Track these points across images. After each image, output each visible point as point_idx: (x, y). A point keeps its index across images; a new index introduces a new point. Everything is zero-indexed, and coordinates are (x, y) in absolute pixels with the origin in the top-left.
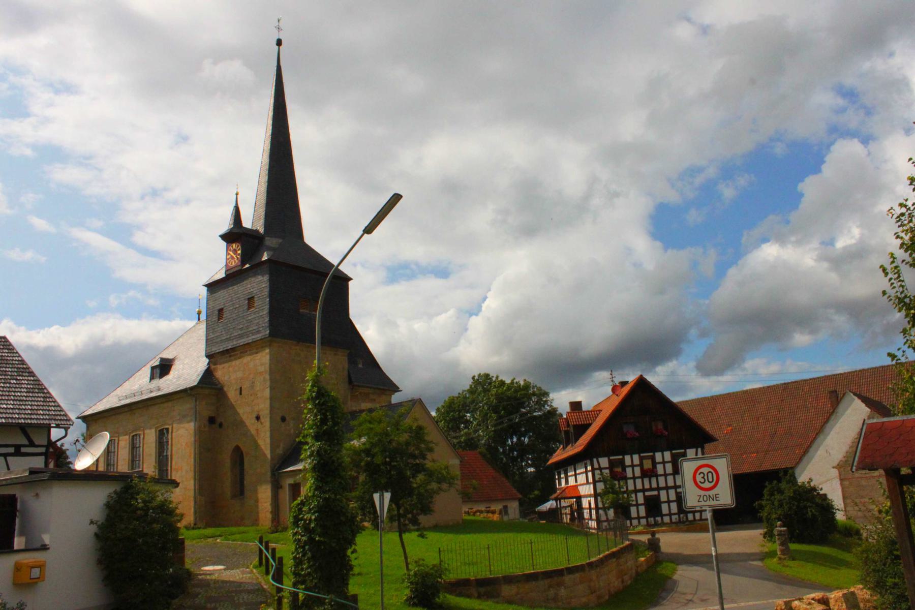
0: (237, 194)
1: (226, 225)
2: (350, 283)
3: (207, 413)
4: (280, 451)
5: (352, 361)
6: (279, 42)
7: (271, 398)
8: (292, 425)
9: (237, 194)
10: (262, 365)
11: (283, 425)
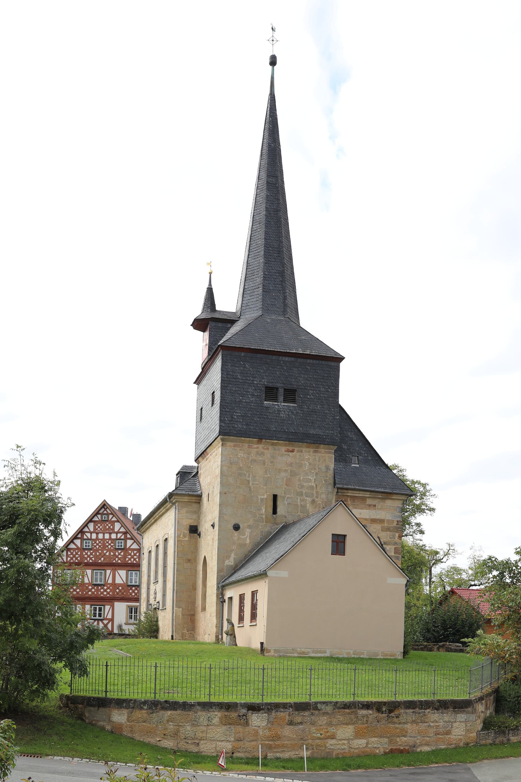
0: (210, 273)
1: (197, 310)
5: (341, 458)
6: (273, 62)
9: (210, 273)
11: (236, 533)
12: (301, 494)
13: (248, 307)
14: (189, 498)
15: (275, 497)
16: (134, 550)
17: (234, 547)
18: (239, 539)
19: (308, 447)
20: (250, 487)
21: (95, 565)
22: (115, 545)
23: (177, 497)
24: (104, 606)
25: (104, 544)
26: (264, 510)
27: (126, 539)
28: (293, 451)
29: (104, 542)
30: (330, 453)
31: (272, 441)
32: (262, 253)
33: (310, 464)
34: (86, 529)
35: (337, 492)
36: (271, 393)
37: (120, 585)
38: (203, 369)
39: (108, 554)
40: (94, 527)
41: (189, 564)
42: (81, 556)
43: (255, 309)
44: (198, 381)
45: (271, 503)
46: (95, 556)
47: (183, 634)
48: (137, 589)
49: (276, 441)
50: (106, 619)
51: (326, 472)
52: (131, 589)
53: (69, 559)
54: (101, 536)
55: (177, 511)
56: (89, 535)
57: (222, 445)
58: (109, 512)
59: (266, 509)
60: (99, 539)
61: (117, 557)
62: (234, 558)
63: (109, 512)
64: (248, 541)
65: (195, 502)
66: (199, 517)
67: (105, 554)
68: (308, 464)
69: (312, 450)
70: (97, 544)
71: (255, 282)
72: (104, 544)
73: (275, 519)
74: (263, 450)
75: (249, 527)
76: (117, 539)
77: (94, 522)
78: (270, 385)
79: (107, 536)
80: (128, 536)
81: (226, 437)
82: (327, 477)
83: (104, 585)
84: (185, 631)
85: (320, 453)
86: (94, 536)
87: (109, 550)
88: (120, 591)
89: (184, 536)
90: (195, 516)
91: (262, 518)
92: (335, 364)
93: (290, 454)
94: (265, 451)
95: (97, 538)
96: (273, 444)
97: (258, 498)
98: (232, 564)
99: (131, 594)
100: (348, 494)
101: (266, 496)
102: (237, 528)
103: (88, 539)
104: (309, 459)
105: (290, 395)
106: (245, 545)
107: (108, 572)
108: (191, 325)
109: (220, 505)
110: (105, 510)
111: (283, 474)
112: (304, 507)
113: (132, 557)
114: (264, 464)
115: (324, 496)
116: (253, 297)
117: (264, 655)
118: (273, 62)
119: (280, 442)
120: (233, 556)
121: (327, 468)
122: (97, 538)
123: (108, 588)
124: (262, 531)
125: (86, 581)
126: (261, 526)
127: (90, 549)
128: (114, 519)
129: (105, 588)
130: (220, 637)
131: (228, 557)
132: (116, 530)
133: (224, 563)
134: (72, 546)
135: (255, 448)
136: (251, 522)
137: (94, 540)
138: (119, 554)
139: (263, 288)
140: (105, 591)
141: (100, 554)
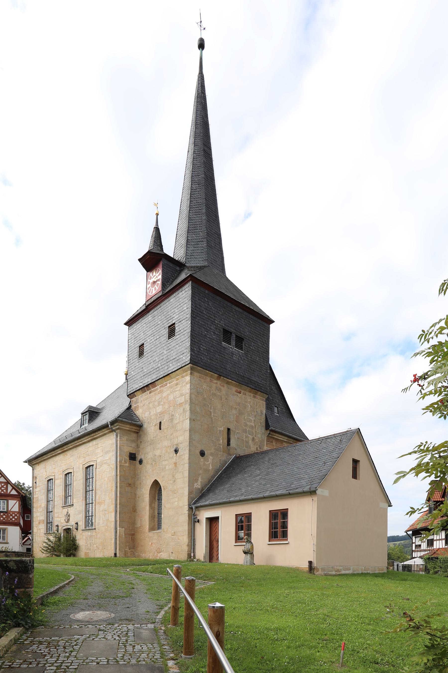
0: (157, 214)
1: (145, 247)
2: (271, 326)
3: (129, 449)
4: (198, 485)
5: (269, 407)
6: (201, 46)
7: (191, 430)
8: (210, 461)
9: (157, 214)
11: (202, 459)
13: (193, 257)
14: (131, 427)
15: (229, 429)
17: (201, 472)
18: (204, 464)
19: (250, 392)
20: (212, 418)
23: (120, 424)
26: (221, 441)
30: (263, 400)
31: (228, 380)
32: (204, 211)
33: (251, 407)
35: (269, 434)
36: (227, 335)
38: (147, 307)
41: (129, 488)
43: (200, 259)
44: (130, 323)
47: (125, 551)
48: (5, 515)
49: (230, 381)
51: (261, 415)
55: (119, 437)
57: (191, 374)
59: (222, 441)
64: (211, 467)
65: (134, 432)
66: (138, 447)
68: (250, 406)
69: (252, 395)
71: (198, 235)
73: (229, 450)
74: (220, 386)
75: (212, 454)
78: (227, 328)
81: (195, 366)
82: (261, 420)
84: (127, 549)
85: (257, 399)
89: (125, 462)
90: (134, 445)
91: (220, 447)
92: (266, 324)
93: (239, 394)
94: (222, 388)
96: (228, 383)
97: (217, 429)
98: (200, 487)
99: (11, 519)
100: (275, 437)
101: (223, 428)
102: (202, 454)
104: (250, 402)
105: (240, 341)
106: (209, 470)
108: (140, 260)
109: (190, 430)
112: (248, 442)
114: (221, 400)
115: (259, 436)
117: (314, 574)
118: (201, 46)
119: (233, 382)
120: (200, 479)
124: (220, 460)
126: (220, 455)
130: (192, 554)
131: (197, 480)
133: (194, 485)
135: (214, 383)
136: (213, 451)
139: (207, 243)
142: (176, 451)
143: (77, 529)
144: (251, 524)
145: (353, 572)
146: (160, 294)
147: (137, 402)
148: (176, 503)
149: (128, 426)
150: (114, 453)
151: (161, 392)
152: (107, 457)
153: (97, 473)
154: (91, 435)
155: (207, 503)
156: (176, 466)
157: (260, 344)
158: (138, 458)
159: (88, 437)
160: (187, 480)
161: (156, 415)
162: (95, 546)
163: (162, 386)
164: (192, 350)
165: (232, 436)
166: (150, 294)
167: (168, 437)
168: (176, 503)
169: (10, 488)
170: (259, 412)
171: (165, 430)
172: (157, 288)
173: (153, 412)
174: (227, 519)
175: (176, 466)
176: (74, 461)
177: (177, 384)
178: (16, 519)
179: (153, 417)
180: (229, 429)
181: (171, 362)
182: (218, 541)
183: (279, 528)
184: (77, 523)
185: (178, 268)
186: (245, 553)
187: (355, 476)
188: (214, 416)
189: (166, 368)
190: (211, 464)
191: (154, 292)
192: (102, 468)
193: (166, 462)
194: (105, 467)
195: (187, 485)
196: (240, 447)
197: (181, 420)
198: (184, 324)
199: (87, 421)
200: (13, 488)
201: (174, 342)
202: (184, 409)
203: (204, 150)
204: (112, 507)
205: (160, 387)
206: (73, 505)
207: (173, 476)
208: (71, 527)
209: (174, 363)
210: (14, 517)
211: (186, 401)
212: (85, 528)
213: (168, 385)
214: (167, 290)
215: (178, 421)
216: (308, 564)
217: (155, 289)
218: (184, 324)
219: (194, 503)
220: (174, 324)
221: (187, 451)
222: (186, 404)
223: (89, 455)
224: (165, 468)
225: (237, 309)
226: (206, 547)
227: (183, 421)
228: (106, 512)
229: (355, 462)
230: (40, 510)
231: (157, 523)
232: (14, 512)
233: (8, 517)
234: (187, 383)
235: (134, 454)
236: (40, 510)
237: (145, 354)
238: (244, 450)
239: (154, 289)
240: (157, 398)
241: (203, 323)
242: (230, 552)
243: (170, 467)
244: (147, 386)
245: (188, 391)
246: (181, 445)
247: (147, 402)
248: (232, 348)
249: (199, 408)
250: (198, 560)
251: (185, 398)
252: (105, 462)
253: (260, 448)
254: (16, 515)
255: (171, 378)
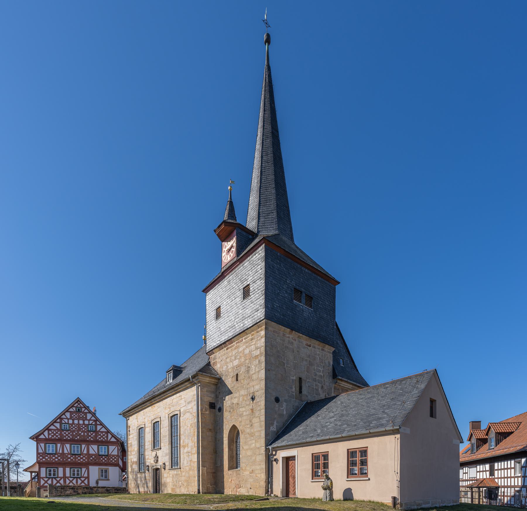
4: (273, 428)
10: (257, 348)
11: (277, 405)
12: (315, 380)
14: (211, 380)
15: (300, 379)
16: (102, 432)
19: (319, 345)
20: (285, 368)
21: (72, 441)
22: (88, 428)
24: (81, 468)
25: (79, 427)
27: (96, 425)
28: (310, 346)
29: (79, 426)
30: (330, 353)
33: (320, 358)
34: (64, 417)
36: (297, 292)
37: (93, 455)
39: (82, 434)
40: (71, 415)
42: (61, 434)
45: (298, 384)
46: (72, 435)
50: (83, 477)
52: (102, 457)
53: (50, 436)
54: (76, 422)
56: (66, 421)
58: (82, 406)
59: (294, 389)
60: (75, 424)
61: (90, 436)
62: (276, 426)
63: (82, 406)
64: (285, 413)
67: (80, 434)
69: (321, 348)
70: (74, 427)
72: (79, 427)
75: (286, 401)
76: (89, 424)
77: (70, 412)
79: (81, 422)
80: (98, 423)
83: (80, 455)
86: (71, 422)
87: (84, 432)
88: (93, 458)
89: (206, 410)
93: (309, 348)
95: (73, 423)
102: (277, 400)
103: (66, 423)
104: (319, 354)
105: (310, 299)
107: (83, 446)
110: (79, 404)
111: (304, 362)
112: (317, 390)
113: (102, 437)
114: (293, 352)
115: (327, 384)
116: (267, 219)
120: (275, 422)
121: (329, 363)
122: (73, 423)
123: (84, 457)
125: (66, 451)
127: (68, 430)
128: (86, 411)
129: (82, 456)
131: (272, 424)
132: (88, 418)
134: (52, 427)
137: (70, 424)
138: (92, 434)
140: (82, 458)
141: (76, 434)
142: (253, 399)
143: (165, 469)
144: (328, 463)
145: (432, 505)
146: (235, 260)
147: (215, 359)
148: (254, 445)
149: (208, 379)
150: (196, 403)
151: (238, 347)
152: (189, 407)
153: (181, 421)
154: (174, 389)
155: (284, 444)
156: (253, 412)
157: (327, 303)
158: (218, 407)
159: (173, 390)
160: (263, 423)
161: (233, 368)
162: (180, 482)
163: (238, 342)
164: (266, 307)
165: (303, 384)
166: (226, 261)
167: (244, 386)
168: (254, 445)
169: (110, 436)
170: (327, 363)
171: (242, 381)
172: (232, 255)
173: (230, 365)
174: (303, 458)
175: (253, 412)
176: (161, 410)
177: (252, 339)
178: (115, 461)
179: (230, 370)
180: (300, 379)
181: (246, 319)
182: (294, 478)
183: (357, 464)
184: (164, 464)
185: (250, 237)
186: (325, 489)
187: (432, 414)
188: (287, 366)
189: (242, 325)
190: (285, 410)
191: (229, 259)
192: (185, 416)
193: (244, 409)
194: (188, 415)
195: (264, 428)
196: (309, 396)
197: (257, 370)
198: (258, 284)
199: (172, 377)
200: (113, 436)
201: (249, 301)
202: (259, 361)
203: (272, 133)
204: (195, 450)
205: (236, 343)
206: (161, 448)
207: (250, 421)
208: (159, 467)
209: (249, 320)
210: (113, 459)
211: (261, 354)
212: (172, 467)
213: (244, 340)
214: (241, 256)
215: (254, 372)
216: (391, 499)
217: (230, 256)
218: (258, 284)
219: (271, 444)
220: (249, 285)
221: (263, 398)
222: (261, 356)
223: (173, 406)
224: (242, 414)
225: (306, 270)
226: (283, 483)
227: (258, 372)
228: (190, 454)
229: (432, 402)
230: (134, 453)
231: (235, 464)
232: (113, 456)
233: (108, 459)
234: (262, 337)
235: (214, 404)
236: (134, 453)
237: (221, 315)
238: (315, 397)
239: (229, 256)
240: (234, 353)
241: (276, 283)
242: (307, 488)
243: (247, 413)
244: (224, 343)
245: (263, 344)
246: (257, 393)
247: (224, 358)
248: (302, 305)
249: (273, 358)
250: (275, 495)
251: (260, 350)
252: (188, 411)
253: (328, 395)
254: (115, 458)
255: (247, 334)
